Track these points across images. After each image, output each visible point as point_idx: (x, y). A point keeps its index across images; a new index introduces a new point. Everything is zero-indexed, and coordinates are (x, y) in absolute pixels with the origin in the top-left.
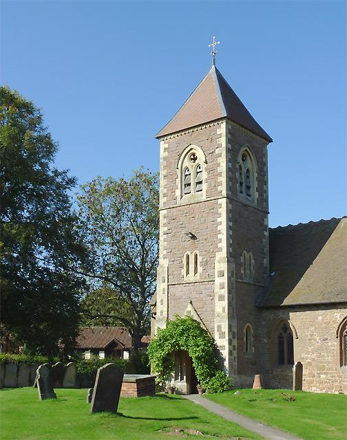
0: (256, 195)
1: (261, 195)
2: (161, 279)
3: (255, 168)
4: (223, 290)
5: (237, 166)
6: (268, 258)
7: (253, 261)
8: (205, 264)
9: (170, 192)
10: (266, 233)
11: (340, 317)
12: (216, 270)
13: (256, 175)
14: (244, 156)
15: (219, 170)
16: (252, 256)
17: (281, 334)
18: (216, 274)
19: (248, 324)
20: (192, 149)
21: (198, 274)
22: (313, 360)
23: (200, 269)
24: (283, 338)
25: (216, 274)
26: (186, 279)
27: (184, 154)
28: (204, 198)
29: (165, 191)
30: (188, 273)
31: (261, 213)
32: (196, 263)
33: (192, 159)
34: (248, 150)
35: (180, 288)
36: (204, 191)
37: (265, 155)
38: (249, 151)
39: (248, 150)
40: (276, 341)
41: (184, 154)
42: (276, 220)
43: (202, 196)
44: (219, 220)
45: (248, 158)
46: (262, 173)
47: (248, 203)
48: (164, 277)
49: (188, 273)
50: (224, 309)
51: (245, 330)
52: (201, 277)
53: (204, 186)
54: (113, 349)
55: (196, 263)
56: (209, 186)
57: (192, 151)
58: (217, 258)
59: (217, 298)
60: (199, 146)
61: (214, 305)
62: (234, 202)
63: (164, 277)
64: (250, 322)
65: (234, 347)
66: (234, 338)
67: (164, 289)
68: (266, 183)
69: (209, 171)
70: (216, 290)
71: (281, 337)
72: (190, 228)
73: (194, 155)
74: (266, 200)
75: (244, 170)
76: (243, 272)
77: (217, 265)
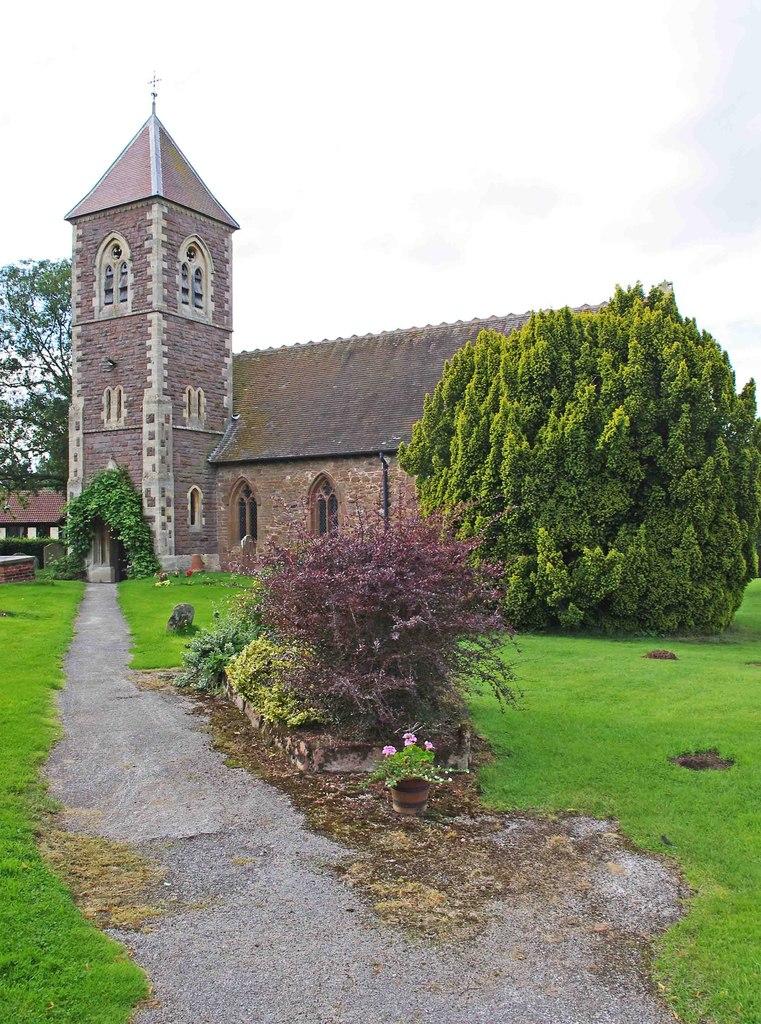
0: (211, 306)
1: (220, 305)
2: (74, 426)
3: (211, 268)
4: (152, 442)
5: (179, 266)
6: (230, 395)
7: (204, 400)
8: (129, 405)
9: (85, 300)
10: (229, 361)
11: (312, 476)
12: (145, 413)
13: (211, 278)
14: (191, 250)
15: (149, 271)
16: (202, 393)
17: (242, 499)
18: (144, 418)
19: (193, 488)
20: (113, 239)
21: (122, 419)
22: (280, 533)
23: (124, 412)
24: (245, 504)
25: (144, 418)
26: (107, 426)
27: (103, 246)
28: (129, 312)
29: (79, 299)
30: (109, 417)
31: (221, 333)
32: (119, 403)
33: (115, 254)
34: (198, 242)
35: (100, 438)
36: (129, 303)
37: (228, 249)
38: (200, 244)
39: (198, 242)
40: (237, 508)
41: (103, 246)
42: (245, 339)
43: (126, 308)
44: (148, 343)
45: (199, 252)
46: (221, 275)
47: (197, 318)
48: (77, 423)
49: (109, 417)
50: (154, 466)
51: (189, 495)
52: (126, 424)
53: (130, 295)
54: (547, 471)
55: (119, 403)
56: (137, 295)
57: (115, 242)
58: (146, 398)
59: (145, 452)
60: (123, 235)
61: (141, 460)
62: (172, 318)
63: (77, 423)
64: (197, 483)
65: (169, 518)
66: (169, 505)
67: (78, 440)
68: (228, 289)
69: (136, 272)
70: (144, 442)
71: (242, 503)
72: (111, 353)
73: (117, 247)
74: (229, 314)
75: (192, 271)
76: (186, 415)
77: (145, 406)
